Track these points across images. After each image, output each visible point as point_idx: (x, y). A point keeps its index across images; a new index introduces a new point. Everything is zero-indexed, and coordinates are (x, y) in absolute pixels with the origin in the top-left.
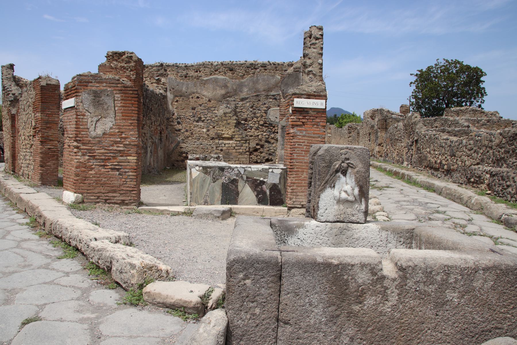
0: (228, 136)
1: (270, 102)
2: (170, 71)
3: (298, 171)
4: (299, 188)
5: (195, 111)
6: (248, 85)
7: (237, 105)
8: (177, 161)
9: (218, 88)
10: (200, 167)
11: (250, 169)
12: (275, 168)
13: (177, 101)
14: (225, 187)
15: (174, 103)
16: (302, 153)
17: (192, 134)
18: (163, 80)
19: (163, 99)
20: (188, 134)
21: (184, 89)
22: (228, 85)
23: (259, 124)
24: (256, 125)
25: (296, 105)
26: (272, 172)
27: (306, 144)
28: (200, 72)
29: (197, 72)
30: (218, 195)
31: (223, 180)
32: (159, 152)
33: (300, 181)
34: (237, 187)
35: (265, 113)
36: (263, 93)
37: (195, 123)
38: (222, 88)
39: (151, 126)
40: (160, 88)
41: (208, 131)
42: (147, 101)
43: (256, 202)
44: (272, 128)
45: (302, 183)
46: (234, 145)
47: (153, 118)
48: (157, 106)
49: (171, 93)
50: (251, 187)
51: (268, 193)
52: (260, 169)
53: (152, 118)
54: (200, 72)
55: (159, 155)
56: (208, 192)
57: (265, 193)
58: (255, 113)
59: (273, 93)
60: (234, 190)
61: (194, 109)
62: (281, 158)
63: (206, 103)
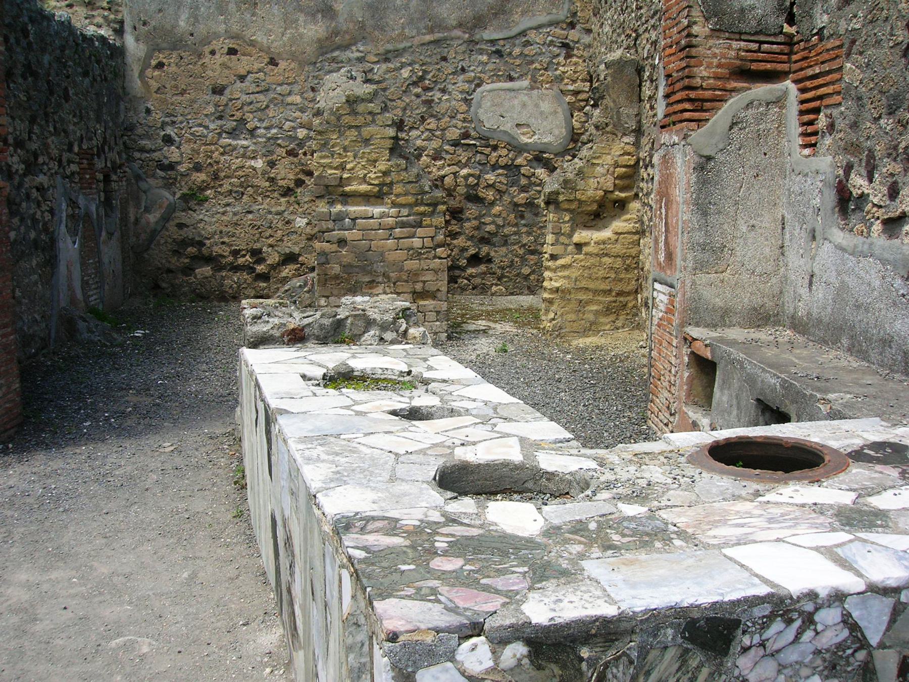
0: (364, 188)
1: (481, 63)
5: (224, 99)
8: (169, 271)
9: (302, 18)
10: (499, 641)
13: (160, 65)
15: (149, 72)
17: (216, 177)
19: (111, 57)
20: (201, 177)
21: (182, 24)
23: (442, 137)
24: (435, 144)
32: (104, 249)
35: (465, 100)
36: (457, 33)
37: (225, 141)
38: (314, 15)
39: (66, 156)
40: (99, 20)
41: (272, 164)
42: (46, 59)
44: (487, 151)
47: (75, 130)
48: (87, 81)
49: (137, 40)
55: (106, 260)
58: (429, 103)
59: (488, 35)
61: (218, 90)
62: (696, 311)
63: (260, 70)
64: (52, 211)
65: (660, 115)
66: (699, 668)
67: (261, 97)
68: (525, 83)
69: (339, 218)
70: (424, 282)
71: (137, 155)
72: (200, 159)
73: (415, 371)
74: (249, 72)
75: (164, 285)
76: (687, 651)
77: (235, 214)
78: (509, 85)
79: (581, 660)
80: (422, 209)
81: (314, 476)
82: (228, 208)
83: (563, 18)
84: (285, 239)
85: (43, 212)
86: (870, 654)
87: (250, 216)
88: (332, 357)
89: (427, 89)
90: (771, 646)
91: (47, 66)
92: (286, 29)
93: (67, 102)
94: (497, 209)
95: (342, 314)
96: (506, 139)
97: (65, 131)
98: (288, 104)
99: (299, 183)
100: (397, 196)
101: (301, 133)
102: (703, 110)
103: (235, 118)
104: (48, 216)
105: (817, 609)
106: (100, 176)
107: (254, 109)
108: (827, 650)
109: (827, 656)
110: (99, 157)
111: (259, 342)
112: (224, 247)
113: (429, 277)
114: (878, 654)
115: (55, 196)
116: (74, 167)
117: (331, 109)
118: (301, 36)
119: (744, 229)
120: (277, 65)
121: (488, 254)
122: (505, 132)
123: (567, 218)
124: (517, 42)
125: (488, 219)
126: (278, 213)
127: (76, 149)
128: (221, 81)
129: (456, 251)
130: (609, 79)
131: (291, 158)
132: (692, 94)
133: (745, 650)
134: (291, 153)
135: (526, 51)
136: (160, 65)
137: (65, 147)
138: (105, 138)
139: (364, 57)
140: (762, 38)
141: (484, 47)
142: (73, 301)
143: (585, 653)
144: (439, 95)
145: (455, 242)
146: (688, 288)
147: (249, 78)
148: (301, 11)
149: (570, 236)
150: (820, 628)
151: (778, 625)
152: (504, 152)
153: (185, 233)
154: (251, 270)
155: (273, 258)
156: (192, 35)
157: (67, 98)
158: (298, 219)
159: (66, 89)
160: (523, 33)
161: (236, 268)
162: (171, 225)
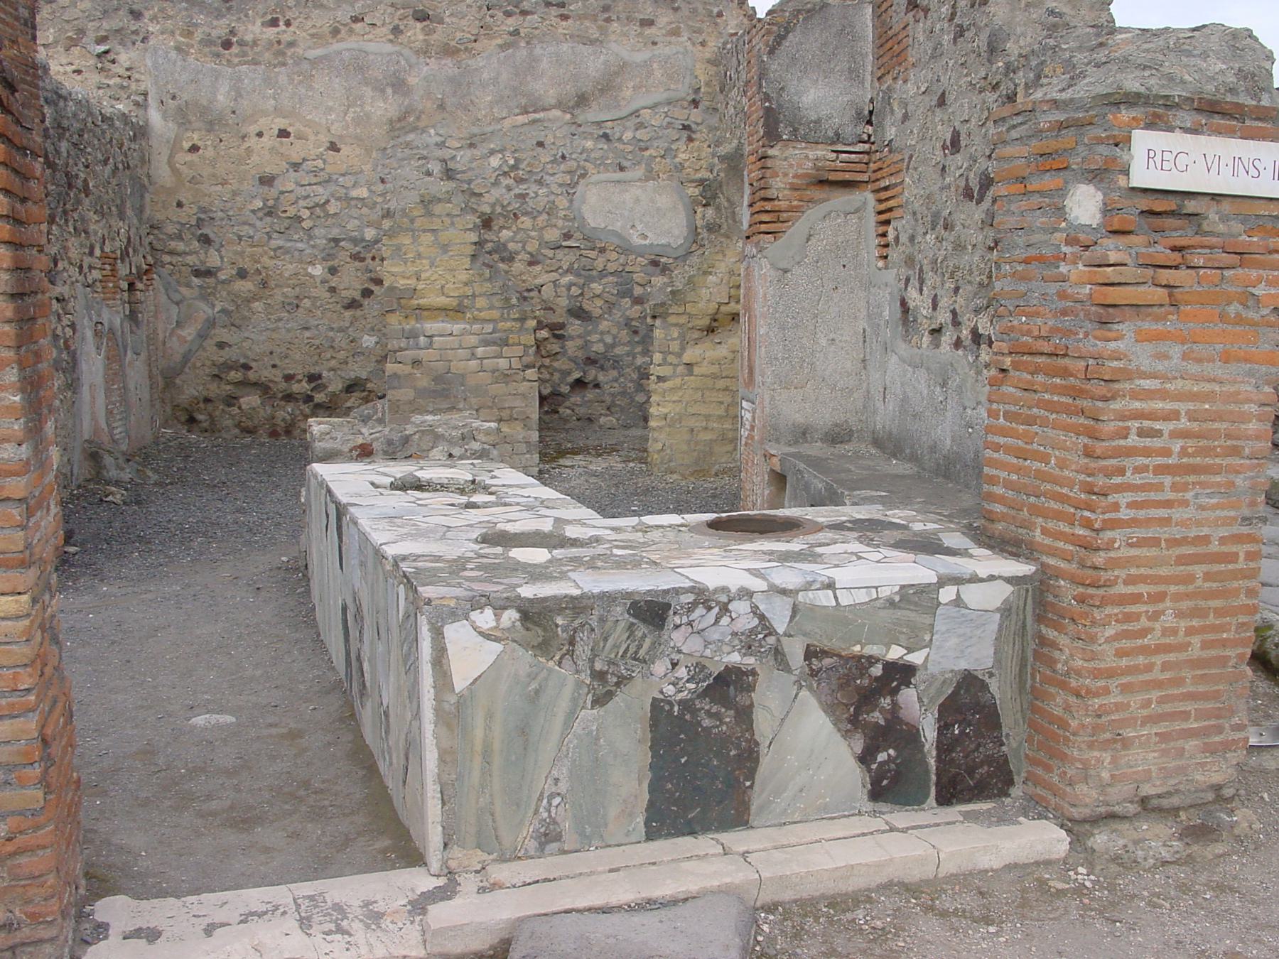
0: (441, 301)
2: (154, 19)
3: (1136, 598)
4: (1136, 700)
5: (274, 192)
6: (495, 81)
7: (451, 165)
9: (368, 92)
11: (825, 599)
12: (975, 579)
13: (194, 149)
14: (670, 729)
16: (1159, 487)
18: (125, 57)
19: (134, 139)
21: (220, 98)
22: (413, 80)
25: (1142, 176)
26: (958, 602)
27: (1184, 423)
28: (288, 24)
29: (274, 23)
30: (630, 783)
31: (665, 680)
32: (130, 372)
33: (1141, 660)
34: (745, 715)
36: (556, 113)
39: (87, 261)
41: (333, 271)
42: (64, 146)
43: (862, 794)
44: (593, 254)
45: (1149, 668)
46: (473, 340)
47: (97, 227)
49: (165, 118)
50: (830, 709)
51: (929, 733)
52: (885, 592)
53: (92, 227)
54: (288, 24)
55: (132, 386)
56: (563, 772)
57: (912, 736)
60: (725, 740)
61: (267, 181)
63: (319, 156)
64: (73, 326)
65: (745, 225)
66: (644, 636)
67: (320, 190)
68: (639, 172)
69: (413, 335)
70: (511, 408)
71: (167, 258)
72: (247, 264)
73: (478, 479)
74: (304, 160)
75: (201, 417)
76: (633, 624)
77: (288, 331)
78: (619, 175)
79: (557, 626)
80: (509, 324)
81: (378, 537)
82: (280, 324)
83: (684, 95)
84: (350, 359)
85: (63, 328)
86: (778, 640)
87: (307, 334)
88: (399, 470)
89: (520, 181)
90: (697, 626)
91: (65, 155)
92: (349, 106)
93: (87, 196)
94: (604, 325)
95: (410, 430)
96: (616, 241)
97: (86, 232)
98: (353, 199)
99: (367, 293)
100: (480, 310)
101: (370, 234)
102: (778, 221)
103: (288, 214)
104: (69, 331)
105: (730, 601)
106: (125, 285)
107: (312, 204)
108: (743, 634)
109: (743, 638)
110: (123, 260)
111: (329, 457)
112: (274, 371)
113: (518, 403)
114: (784, 640)
115: (77, 308)
116: (96, 274)
117: (403, 210)
118: (368, 115)
119: (824, 342)
120: (338, 150)
121: (595, 379)
122: (615, 233)
123: (676, 335)
124: (628, 124)
125: (595, 337)
126: (341, 330)
127: (98, 252)
128: (269, 170)
129: (557, 376)
130: (722, 175)
131: (357, 263)
132: (768, 206)
133: (677, 627)
134: (356, 257)
135: (639, 135)
136: (194, 149)
137: (87, 251)
138: (129, 238)
139: (444, 142)
140: (840, 147)
141: (589, 130)
142: (96, 431)
143: (560, 621)
144: (534, 187)
145: (556, 364)
146: (766, 403)
147: (304, 166)
148: (367, 84)
149: (679, 355)
150: (734, 616)
151: (700, 611)
152: (614, 256)
153: (226, 354)
154: (309, 399)
155: (336, 386)
156: (234, 112)
157: (87, 192)
158: (366, 337)
159: (85, 180)
160: (636, 113)
161: (289, 397)
162: (210, 344)
